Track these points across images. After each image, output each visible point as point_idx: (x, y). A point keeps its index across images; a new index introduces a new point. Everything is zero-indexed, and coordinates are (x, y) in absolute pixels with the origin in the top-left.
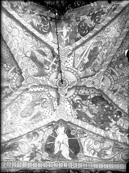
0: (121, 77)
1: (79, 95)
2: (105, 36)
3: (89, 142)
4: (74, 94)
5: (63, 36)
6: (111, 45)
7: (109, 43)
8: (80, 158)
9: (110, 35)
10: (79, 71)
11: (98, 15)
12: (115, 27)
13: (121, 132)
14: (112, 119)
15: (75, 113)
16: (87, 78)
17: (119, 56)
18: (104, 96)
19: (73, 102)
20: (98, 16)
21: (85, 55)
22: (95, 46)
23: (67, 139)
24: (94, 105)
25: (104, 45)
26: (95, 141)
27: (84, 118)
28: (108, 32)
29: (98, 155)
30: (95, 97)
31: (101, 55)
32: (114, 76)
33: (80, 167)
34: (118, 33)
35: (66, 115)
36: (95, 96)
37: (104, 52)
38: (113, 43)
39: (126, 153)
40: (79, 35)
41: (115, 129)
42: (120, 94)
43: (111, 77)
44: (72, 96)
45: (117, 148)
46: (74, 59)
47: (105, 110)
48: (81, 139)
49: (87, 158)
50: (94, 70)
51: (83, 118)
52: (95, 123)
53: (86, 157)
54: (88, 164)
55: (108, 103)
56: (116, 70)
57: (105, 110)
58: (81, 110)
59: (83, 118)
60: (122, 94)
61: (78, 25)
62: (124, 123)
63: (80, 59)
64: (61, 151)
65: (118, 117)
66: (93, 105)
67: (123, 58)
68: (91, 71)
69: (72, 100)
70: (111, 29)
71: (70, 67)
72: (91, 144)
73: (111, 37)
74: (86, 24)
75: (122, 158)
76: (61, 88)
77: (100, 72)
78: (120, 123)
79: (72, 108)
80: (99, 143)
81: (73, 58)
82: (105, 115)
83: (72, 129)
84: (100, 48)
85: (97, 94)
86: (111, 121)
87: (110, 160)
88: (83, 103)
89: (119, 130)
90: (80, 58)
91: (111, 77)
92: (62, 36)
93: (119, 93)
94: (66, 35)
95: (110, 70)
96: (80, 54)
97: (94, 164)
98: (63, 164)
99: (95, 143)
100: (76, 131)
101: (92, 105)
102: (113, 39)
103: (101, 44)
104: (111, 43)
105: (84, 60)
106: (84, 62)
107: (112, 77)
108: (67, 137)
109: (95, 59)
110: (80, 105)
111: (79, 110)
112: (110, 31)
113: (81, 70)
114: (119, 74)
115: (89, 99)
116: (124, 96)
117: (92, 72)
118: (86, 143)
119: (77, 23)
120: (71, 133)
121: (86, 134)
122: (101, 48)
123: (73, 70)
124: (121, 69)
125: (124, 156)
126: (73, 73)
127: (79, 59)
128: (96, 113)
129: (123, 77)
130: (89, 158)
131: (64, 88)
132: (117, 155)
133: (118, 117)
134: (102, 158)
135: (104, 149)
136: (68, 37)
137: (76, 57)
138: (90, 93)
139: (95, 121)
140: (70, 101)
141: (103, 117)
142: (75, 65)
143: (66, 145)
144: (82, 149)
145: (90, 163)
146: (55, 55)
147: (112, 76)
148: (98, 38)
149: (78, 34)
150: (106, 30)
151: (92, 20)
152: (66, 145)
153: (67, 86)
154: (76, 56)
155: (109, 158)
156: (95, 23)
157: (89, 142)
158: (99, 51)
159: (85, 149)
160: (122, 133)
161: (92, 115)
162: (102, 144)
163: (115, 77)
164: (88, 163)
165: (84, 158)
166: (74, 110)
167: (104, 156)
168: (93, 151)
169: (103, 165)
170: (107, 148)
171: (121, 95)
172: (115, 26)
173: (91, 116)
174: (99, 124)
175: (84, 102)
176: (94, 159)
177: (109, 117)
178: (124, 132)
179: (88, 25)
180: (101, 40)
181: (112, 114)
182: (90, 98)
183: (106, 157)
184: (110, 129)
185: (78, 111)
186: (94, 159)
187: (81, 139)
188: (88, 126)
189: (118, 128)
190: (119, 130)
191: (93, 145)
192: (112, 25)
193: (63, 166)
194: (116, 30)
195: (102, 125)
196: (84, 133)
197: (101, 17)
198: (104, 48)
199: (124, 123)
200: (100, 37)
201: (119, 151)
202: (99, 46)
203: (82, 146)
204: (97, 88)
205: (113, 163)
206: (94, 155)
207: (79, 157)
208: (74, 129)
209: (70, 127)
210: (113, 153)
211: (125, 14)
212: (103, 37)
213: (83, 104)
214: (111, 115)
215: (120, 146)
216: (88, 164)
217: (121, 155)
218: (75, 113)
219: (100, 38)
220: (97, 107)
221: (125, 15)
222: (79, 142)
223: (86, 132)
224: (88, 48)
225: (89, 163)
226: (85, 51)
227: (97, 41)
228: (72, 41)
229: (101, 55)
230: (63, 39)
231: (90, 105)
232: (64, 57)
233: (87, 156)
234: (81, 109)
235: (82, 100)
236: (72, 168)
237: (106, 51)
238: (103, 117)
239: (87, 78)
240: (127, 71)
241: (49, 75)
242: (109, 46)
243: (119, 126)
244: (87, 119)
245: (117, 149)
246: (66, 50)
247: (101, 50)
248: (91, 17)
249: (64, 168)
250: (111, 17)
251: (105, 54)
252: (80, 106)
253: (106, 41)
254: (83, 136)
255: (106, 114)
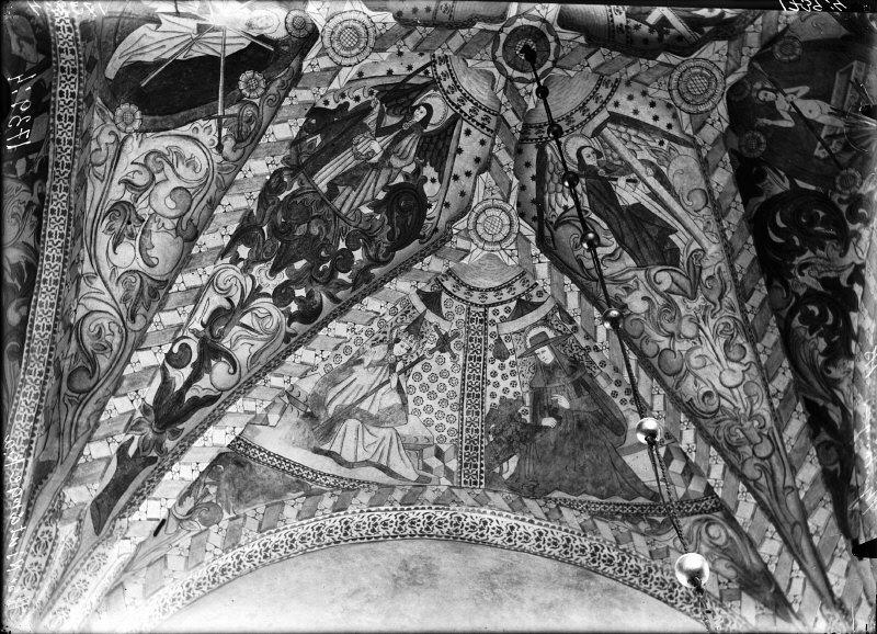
0: (491, 341)
1: (452, 123)
2: (712, 322)
3: (190, 163)
4: (466, 97)
5: (806, 97)
6: (654, 342)
7: (671, 335)
8: (114, 121)
9: (706, 349)
10: (582, 142)
11: (836, 322)
12: (735, 390)
13: (211, 317)
14: (286, 278)
15: (357, 99)
16: (533, 178)
17: (592, 362)
18: (414, 246)
19: (423, 88)
20: (830, 322)
21: (654, 196)
22: (683, 258)
23: (219, 49)
24: (381, 196)
25: (670, 305)
26: (192, 191)
27: (319, 141)
28: (727, 346)
29: (119, 203)
30: (422, 204)
31: (630, 275)
32: (507, 310)
33: (60, 127)
34: (701, 393)
35: (339, 59)
36: (430, 206)
37: (639, 294)
38: (660, 353)
39: (108, 332)
40: (780, 190)
41: (234, 288)
42: (409, 321)
43: (506, 295)
44: (456, 86)
45: (140, 293)
46: (653, 127)
47: (342, 245)
48: (213, 123)
49: (112, 153)
50: (568, 222)
51: (318, 139)
52: (281, 197)
53: (113, 149)
54: (68, 166)
55: (376, 262)
56: (535, 325)
57: (342, 245)
58: (365, 128)
59: (318, 139)
60: (406, 330)
61: (835, 199)
62: (253, 330)
63: (642, 161)
64: (159, 22)
65: (294, 307)
66: (383, 189)
67: (578, 375)
68: (564, 203)
69: (434, 84)
70: (735, 366)
71: (617, 97)
72: (181, 169)
73: (698, 352)
74: (816, 242)
75: (91, 312)
76: (503, 37)
77: (537, 256)
78: (262, 312)
79: (388, 81)
80: (178, 212)
81: (662, 124)
82: (312, 248)
83: (270, 81)
84: (665, 279)
85: (436, 214)
86: (279, 270)
87: (87, 258)
88: (405, 142)
89: (226, 304)
90: (652, 164)
91: (510, 296)
92: (804, 90)
93: (420, 319)
94: (806, 114)
95: (541, 300)
96: (670, 172)
97: (69, 197)
98: (73, 52)
99: (179, 192)
100: (257, 101)
101: (382, 182)
102: (685, 359)
103: (685, 294)
104: (665, 343)
105: (634, 181)
106: (622, 181)
107: (504, 298)
108: (230, 51)
109: (620, 240)
110: (399, 125)
111: (371, 120)
112: (728, 359)
113: (585, 152)
114: (508, 338)
115: (418, 171)
116: (398, 341)
117: (559, 211)
118: (189, 149)
119: (845, 198)
120: (249, 74)
121: (234, 149)
122: (663, 288)
123: (598, 111)
124: (531, 352)
125: (99, 322)
126: (582, 108)
127: (646, 155)
128: (337, 203)
129: (490, 354)
130: (109, 163)
131: (499, 53)
132: (104, 290)
133: (294, 307)
134: (106, 221)
135: (143, 232)
136: (791, 124)
137: (661, 143)
138: (452, 181)
139: (294, 195)
140: (427, 72)
141: (308, 234)
142: (622, 129)
143: (189, 47)
144: (159, 125)
145: (74, 179)
146: (702, 32)
147: (511, 300)
148: (717, 285)
149: (787, 185)
150: (740, 340)
151: (824, 282)
152: (189, 47)
153: (510, 71)
154: (665, 147)
155: (101, 252)
156: (801, 291)
157: (190, 163)
158: (653, 272)
159: (160, 143)
160: (205, 320)
161: (326, 181)
162: (169, 225)
163: (502, 313)
164: (75, 166)
165: (112, 139)
166: (371, 93)
167: (110, 229)
168: (140, 180)
169: (61, 236)
170: (147, 245)
171: (403, 327)
172: (741, 388)
173: (323, 179)
174: (274, 213)
175: (409, 144)
176: (99, 186)
177: (299, 265)
178: (211, 331)
179: (809, 254)
180: (700, 301)
181: (312, 280)
182: (425, 180)
183: (104, 240)
184: (241, 264)
185: (365, 110)
186: (99, 186)
187: (213, 123)
188: (259, 168)
189: (236, 301)
190: (226, 304)
191: (175, 183)
192: (747, 378)
193: (61, 51)
194: (719, 387)
195: (265, 228)
196: (237, 141)
197: (820, 335)
198: (660, 300)
199: (253, 330)
200: (721, 298)
201: (125, 299)
202: (677, 276)
203: (178, 125)
204: (461, 225)
205: (62, 280)
206: (122, 186)
207: (119, 112)
208: (266, 89)
209: (280, 70)
210: (121, 271)
211: (774, 458)
212: (709, 314)
213: (397, 140)
214: (310, 276)
215: (142, 310)
216: (68, 166)
217: (104, 307)
218: (357, 99)
219: (714, 297)
220: (366, 210)
221: (769, 457)
222: (199, 110)
223: (240, 151)
224: (689, 222)
225: (75, 173)
226: (677, 197)
227: (704, 277)
228: (759, 144)
229: (630, 275)
230: (787, 91)
231: (385, 173)
232: (674, 82)
233: (122, 154)
234: (373, 127)
235: (424, 137)
236: (56, 88)
237: (637, 304)
238: (308, 234)
239: (533, 178)
240: (512, 390)
241: (458, 94)
242: (658, 327)
243: (244, 306)
244: (313, 157)
245: (133, 294)
246: (709, 106)
247: (653, 283)
248: (844, 282)
249: (53, 52)
250: (786, 392)
251: (626, 301)
252: (390, 121)
253: (685, 321)
254: (224, 132)
255: (320, 250)
